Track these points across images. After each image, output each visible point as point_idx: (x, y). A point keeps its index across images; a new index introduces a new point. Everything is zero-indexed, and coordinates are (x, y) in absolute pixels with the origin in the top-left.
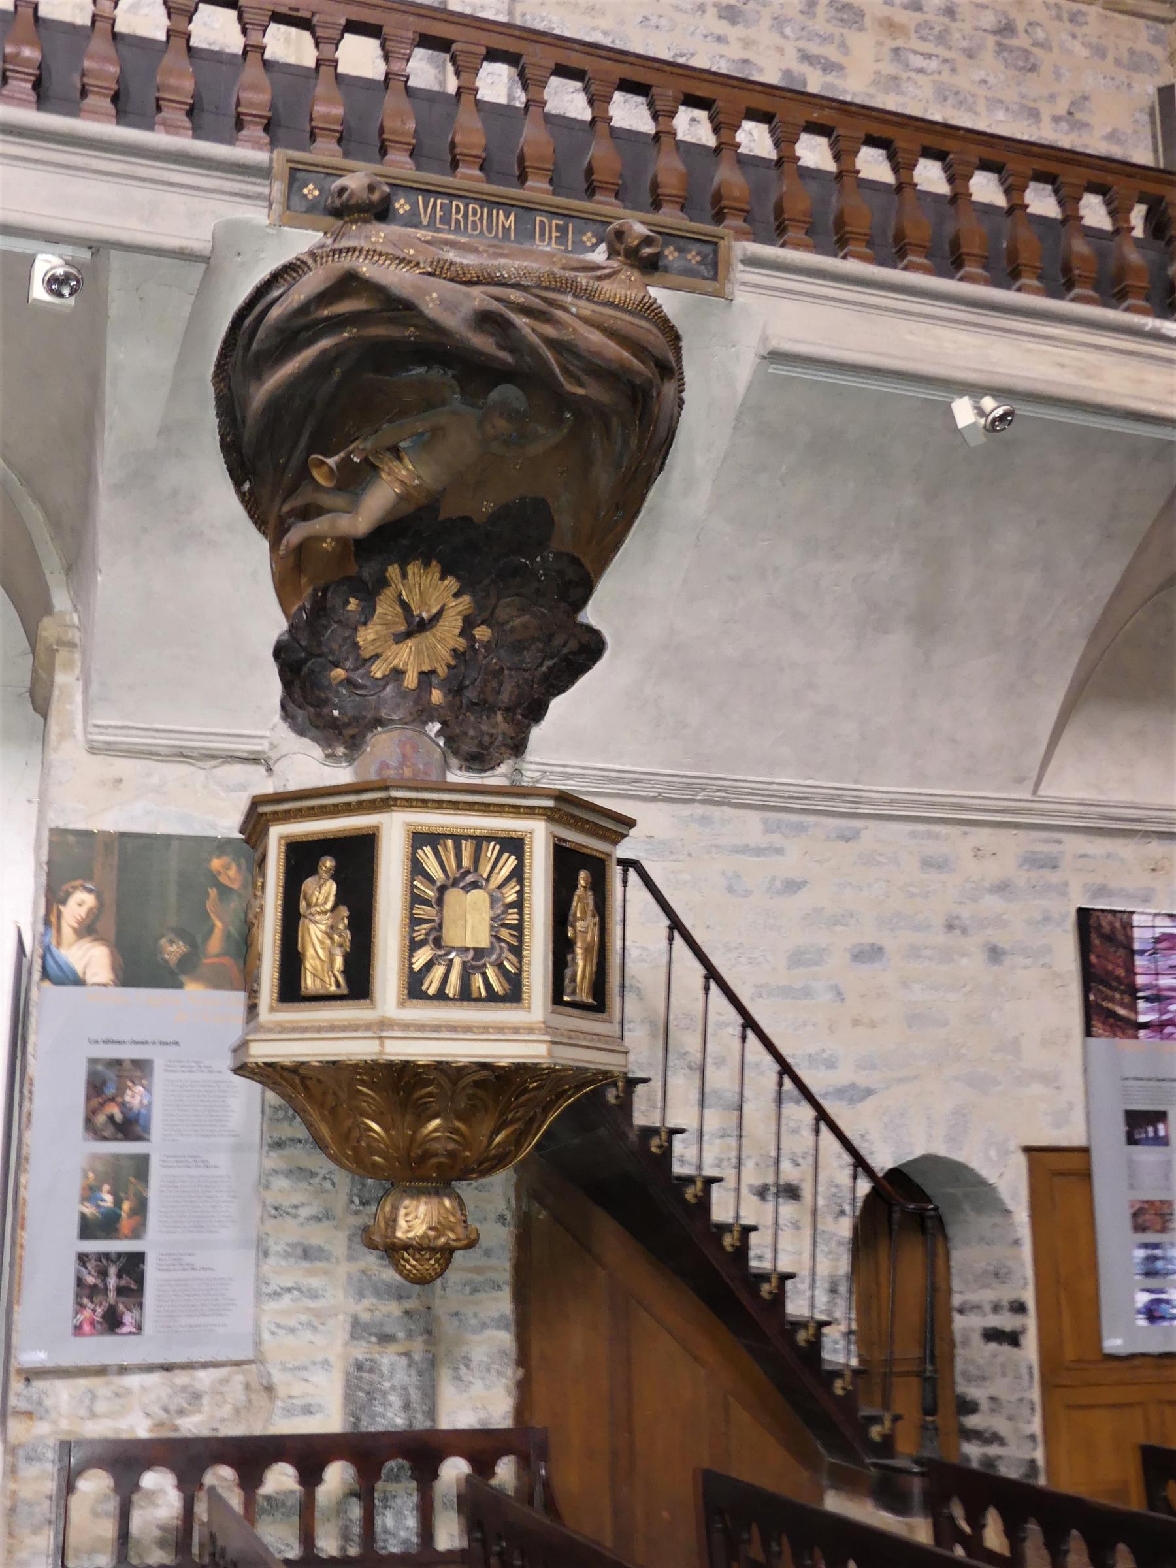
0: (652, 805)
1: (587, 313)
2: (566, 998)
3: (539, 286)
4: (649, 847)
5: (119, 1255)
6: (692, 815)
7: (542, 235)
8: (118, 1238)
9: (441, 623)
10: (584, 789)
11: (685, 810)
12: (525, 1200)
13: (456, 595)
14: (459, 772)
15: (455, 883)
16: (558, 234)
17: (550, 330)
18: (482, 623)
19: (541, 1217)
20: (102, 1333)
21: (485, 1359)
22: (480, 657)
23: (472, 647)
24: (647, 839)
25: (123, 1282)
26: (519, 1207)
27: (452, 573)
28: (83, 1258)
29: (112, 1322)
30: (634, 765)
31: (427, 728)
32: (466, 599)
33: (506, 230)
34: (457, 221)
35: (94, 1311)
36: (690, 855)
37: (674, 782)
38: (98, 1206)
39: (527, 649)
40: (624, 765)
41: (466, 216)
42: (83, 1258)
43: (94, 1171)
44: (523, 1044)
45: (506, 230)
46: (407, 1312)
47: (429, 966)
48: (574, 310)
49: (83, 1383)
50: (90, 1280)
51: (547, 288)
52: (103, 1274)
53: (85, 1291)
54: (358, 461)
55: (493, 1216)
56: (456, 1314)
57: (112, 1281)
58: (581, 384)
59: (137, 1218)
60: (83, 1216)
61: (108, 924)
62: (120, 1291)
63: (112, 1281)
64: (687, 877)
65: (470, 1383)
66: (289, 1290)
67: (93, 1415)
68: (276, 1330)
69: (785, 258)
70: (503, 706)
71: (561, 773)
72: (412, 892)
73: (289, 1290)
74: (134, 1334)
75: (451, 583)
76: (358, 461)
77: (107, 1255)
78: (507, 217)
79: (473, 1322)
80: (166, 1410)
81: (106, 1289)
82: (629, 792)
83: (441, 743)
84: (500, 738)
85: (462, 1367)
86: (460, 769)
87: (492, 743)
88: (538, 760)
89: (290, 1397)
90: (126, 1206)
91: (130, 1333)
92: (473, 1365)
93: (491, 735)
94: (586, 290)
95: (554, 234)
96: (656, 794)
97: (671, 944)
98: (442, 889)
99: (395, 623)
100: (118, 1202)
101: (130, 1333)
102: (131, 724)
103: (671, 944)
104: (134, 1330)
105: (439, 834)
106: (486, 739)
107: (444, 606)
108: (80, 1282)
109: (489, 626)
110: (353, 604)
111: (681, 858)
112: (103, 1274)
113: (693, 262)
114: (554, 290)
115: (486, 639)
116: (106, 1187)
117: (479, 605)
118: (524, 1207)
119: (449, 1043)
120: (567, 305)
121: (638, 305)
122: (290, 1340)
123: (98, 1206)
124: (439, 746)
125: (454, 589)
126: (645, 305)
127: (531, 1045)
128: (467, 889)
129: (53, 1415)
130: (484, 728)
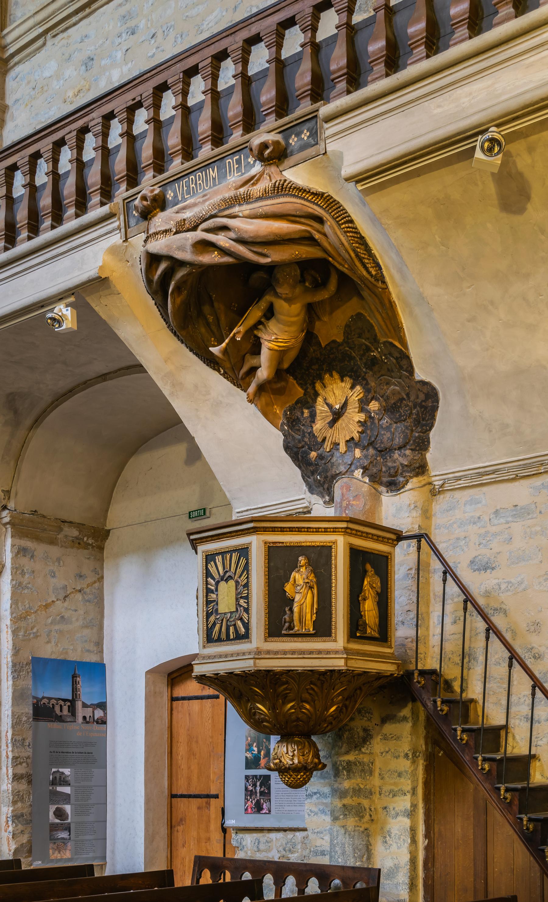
0: (517, 484)
1: (247, 213)
2: (283, 632)
3: (220, 211)
4: (515, 513)
5: (261, 776)
6: (543, 484)
7: (230, 171)
8: (259, 769)
9: (349, 407)
10: (471, 484)
11: (537, 482)
12: (430, 745)
13: (352, 388)
14: (387, 494)
15: (222, 580)
16: (237, 166)
17: (232, 235)
18: (371, 400)
19: (440, 755)
20: (254, 813)
21: (398, 832)
22: (376, 421)
23: (370, 417)
24: (514, 508)
25: (262, 789)
26: (427, 749)
27: (346, 375)
28: (247, 778)
29: (258, 808)
30: (490, 461)
31: (355, 474)
32: (358, 388)
33: (214, 179)
34: (193, 188)
35: (251, 802)
36: (540, 512)
37: (520, 465)
38: (252, 753)
39: (400, 407)
40: (485, 462)
41: (196, 184)
42: (247, 778)
43: (250, 737)
44: (244, 661)
45: (214, 179)
46: (344, 805)
47: (214, 624)
48: (241, 215)
49: (255, 835)
50: (250, 788)
51: (224, 210)
52: (255, 785)
53: (249, 793)
54: (239, 339)
55: (402, 754)
56: (385, 808)
57: (258, 788)
58: (265, 256)
59: (267, 758)
60: (246, 757)
62: (262, 793)
63: (258, 788)
64: (538, 528)
65: (391, 845)
66: (315, 793)
67: (259, 850)
68: (310, 813)
69: (341, 106)
70: (397, 447)
71: (453, 477)
72: (207, 588)
73: (315, 793)
74: (267, 813)
75: (348, 382)
76: (239, 339)
77: (256, 776)
78: (213, 171)
79: (393, 812)
80: (284, 850)
81: (256, 792)
82: (497, 479)
83: (367, 481)
84: (401, 468)
85: (387, 836)
86: (387, 492)
87: (396, 472)
88: (438, 473)
89: (316, 846)
90: (262, 753)
91: (265, 813)
92: (393, 835)
93: (394, 467)
94: (244, 197)
95: (236, 166)
96: (514, 476)
97: (444, 584)
98: (217, 583)
99: (327, 416)
100: (259, 752)
101: (265, 813)
102: (249, 508)
103: (444, 584)
104: (267, 812)
105: (214, 554)
106: (392, 471)
107: (347, 397)
108: (246, 789)
109: (376, 400)
110: (306, 412)
111: (535, 516)
112: (255, 785)
113: (306, 138)
114: (228, 208)
115: (377, 409)
116: (255, 744)
117: (367, 390)
118: (430, 750)
119: (217, 664)
120: (236, 214)
121: (274, 190)
122: (315, 818)
124: (365, 483)
125: (349, 386)
126: (278, 187)
127: (247, 661)
128: (227, 581)
129: (245, 849)
130: (390, 464)
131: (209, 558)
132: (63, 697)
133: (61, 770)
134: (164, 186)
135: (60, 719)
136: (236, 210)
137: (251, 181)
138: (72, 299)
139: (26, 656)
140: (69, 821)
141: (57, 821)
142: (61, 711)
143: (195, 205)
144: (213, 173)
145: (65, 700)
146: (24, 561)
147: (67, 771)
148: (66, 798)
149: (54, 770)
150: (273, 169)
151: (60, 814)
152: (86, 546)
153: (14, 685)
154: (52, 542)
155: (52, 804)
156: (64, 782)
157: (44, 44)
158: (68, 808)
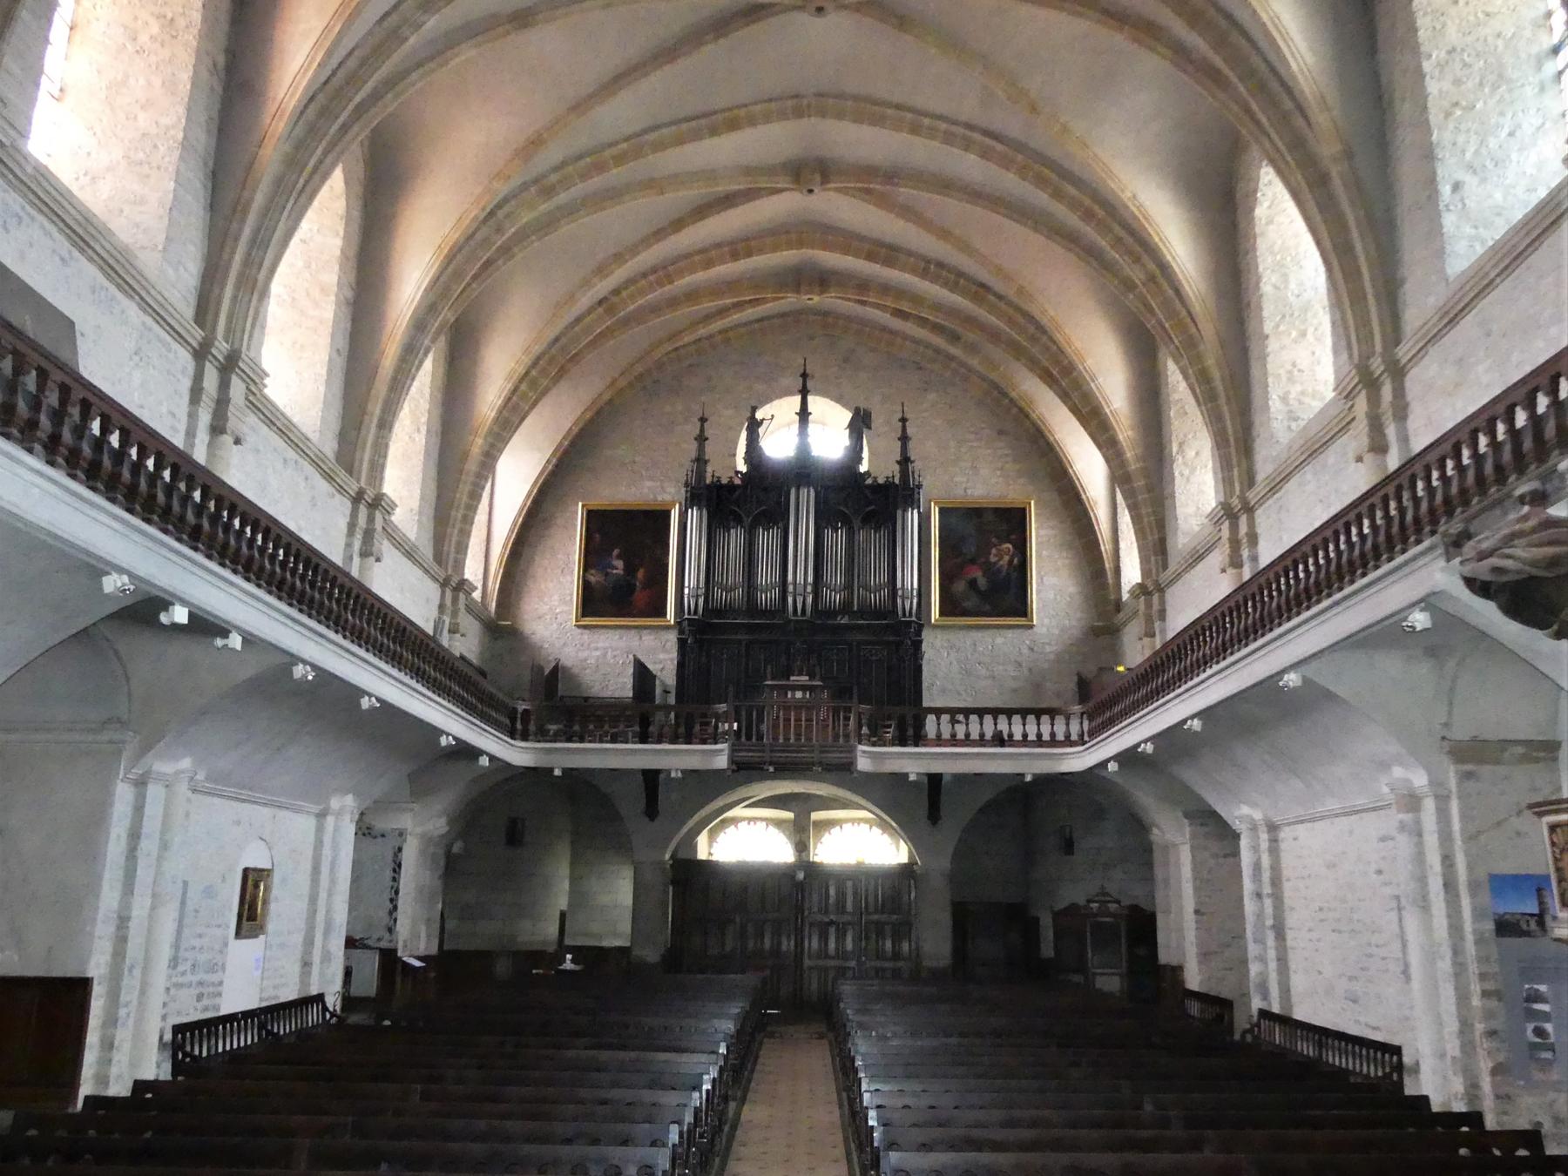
38: (607, 574)
123: (607, 574)
131: (1553, 828)
132: (1529, 912)
133: (1535, 986)
134: (1468, 521)
135: (1527, 934)
136: (1516, 542)
137: (1525, 518)
138: (1423, 605)
139: (1482, 874)
140: (1552, 1040)
141: (1538, 1040)
142: (1528, 925)
143: (1487, 538)
144: (1498, 512)
145: (1532, 915)
146: (1471, 785)
147: (1543, 988)
148: (1546, 1017)
149: (1527, 986)
150: (1538, 509)
151: (1540, 1032)
152: (1537, 760)
153: (1472, 903)
154: (1497, 762)
155: (1529, 1022)
156: (1538, 998)
157: (1426, 353)
158: (1549, 1027)
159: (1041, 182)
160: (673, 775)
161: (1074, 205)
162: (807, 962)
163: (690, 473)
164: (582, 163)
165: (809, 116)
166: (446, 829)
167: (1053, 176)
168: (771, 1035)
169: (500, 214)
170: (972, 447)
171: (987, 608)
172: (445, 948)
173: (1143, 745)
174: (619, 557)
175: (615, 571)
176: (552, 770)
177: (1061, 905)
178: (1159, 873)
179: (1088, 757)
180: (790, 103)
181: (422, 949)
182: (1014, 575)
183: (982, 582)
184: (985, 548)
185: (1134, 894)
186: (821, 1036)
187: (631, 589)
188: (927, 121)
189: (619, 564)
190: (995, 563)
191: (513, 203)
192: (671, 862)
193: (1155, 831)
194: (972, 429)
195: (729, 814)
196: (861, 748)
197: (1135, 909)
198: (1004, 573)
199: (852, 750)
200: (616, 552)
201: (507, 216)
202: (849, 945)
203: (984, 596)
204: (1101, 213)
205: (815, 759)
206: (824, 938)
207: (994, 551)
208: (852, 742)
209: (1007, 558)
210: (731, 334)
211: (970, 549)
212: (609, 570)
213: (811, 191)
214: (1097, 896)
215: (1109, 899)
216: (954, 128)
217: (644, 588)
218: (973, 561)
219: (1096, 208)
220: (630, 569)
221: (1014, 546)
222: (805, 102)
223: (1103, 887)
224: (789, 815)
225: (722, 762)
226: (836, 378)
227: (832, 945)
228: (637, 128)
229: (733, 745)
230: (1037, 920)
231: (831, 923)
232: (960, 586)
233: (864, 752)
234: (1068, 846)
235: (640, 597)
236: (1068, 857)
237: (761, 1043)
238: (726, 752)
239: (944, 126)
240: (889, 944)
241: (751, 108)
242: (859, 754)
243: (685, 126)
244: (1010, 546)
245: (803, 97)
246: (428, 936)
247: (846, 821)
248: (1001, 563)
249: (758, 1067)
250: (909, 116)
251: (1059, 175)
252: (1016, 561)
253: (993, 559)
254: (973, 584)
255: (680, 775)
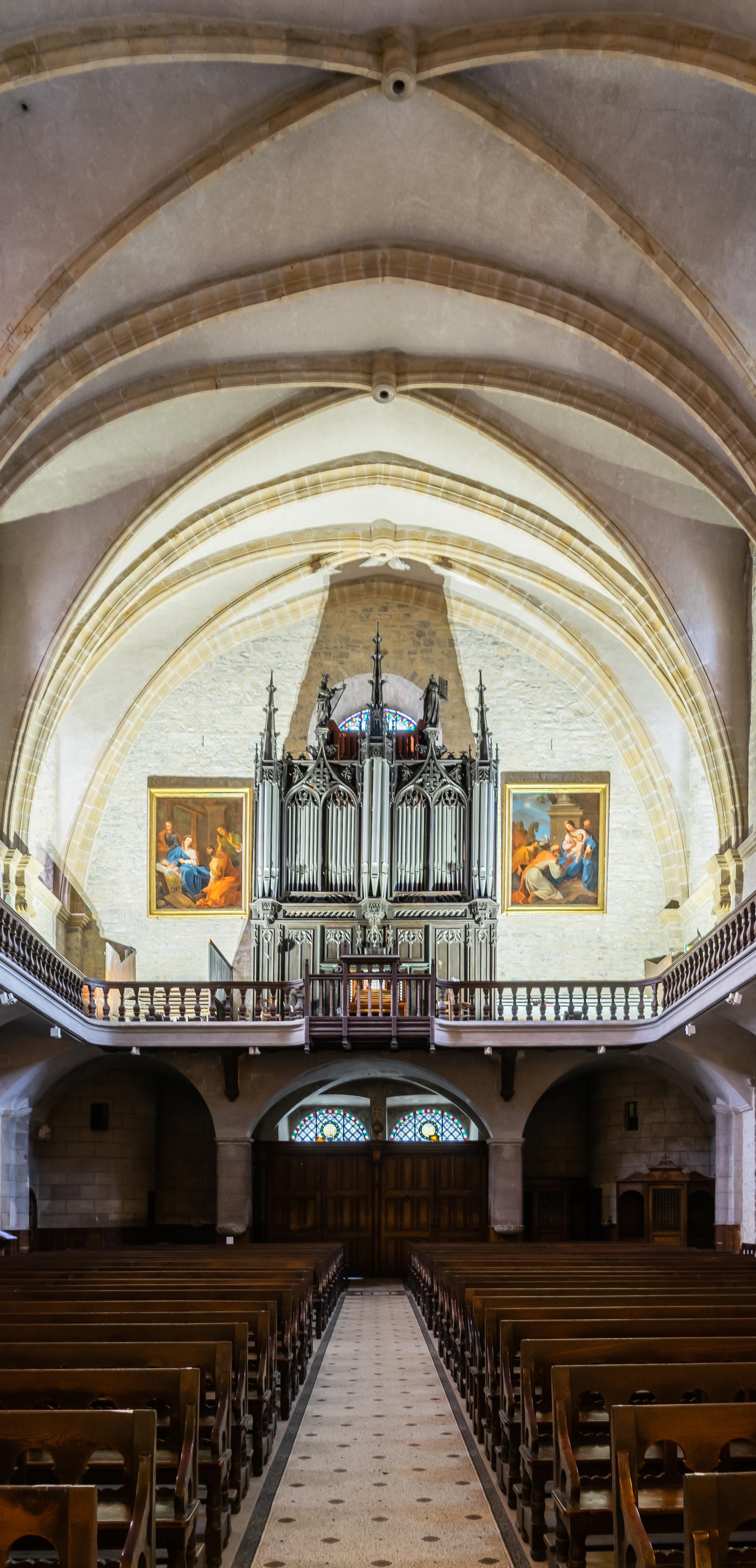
38: (179, 865)
61: (195, 845)
159: (648, 360)
160: (251, 1052)
161: (685, 390)
162: (384, 1234)
163: (259, 747)
164: (119, 328)
165: (384, 275)
166: (29, 1110)
167: (665, 353)
168: (353, 1294)
169: (27, 391)
170: (547, 729)
171: (559, 896)
172: (39, 1226)
173: (731, 995)
174: (190, 846)
175: (187, 862)
176: (130, 1049)
177: (624, 1175)
178: (720, 1140)
179: (662, 1027)
180: (360, 255)
181: (13, 1225)
182: (587, 862)
183: (556, 872)
184: (557, 834)
185: (693, 1163)
186: (400, 1293)
187: (205, 882)
188: (520, 281)
189: (192, 854)
190: (569, 850)
191: (41, 376)
192: (252, 1140)
193: (719, 1101)
194: (549, 710)
195: (308, 1101)
196: (438, 1021)
197: (694, 1175)
198: (576, 861)
199: (428, 1024)
200: (188, 840)
201: (37, 394)
202: (423, 1217)
203: (556, 884)
204: (713, 397)
205: (392, 1034)
206: (399, 1211)
207: (567, 837)
208: (429, 1015)
209: (580, 845)
210: (299, 604)
211: (543, 836)
212: (182, 861)
213: (384, 395)
214: (660, 1164)
215: (672, 1167)
216: (552, 290)
217: (219, 878)
218: (546, 847)
219: (710, 391)
220: (204, 860)
221: (587, 832)
222: (379, 254)
223: (666, 1157)
224: (365, 1101)
225: (299, 1037)
226: (409, 653)
227: (407, 1219)
228: (182, 278)
229: (311, 1020)
230: (599, 1191)
231: (407, 1198)
232: (532, 875)
233: (441, 1025)
234: (632, 1124)
235: (215, 888)
236: (631, 1132)
237: (343, 1298)
238: (304, 1027)
239: (539, 286)
240: (460, 1217)
241: (317, 261)
242: (436, 1027)
243: (238, 283)
244: (583, 832)
245: (376, 247)
246: (19, 1213)
247: (413, 1108)
248: (574, 850)
249: (341, 1315)
250: (500, 273)
251: (671, 350)
252: (588, 849)
253: (566, 846)
254: (546, 872)
255: (258, 1052)
